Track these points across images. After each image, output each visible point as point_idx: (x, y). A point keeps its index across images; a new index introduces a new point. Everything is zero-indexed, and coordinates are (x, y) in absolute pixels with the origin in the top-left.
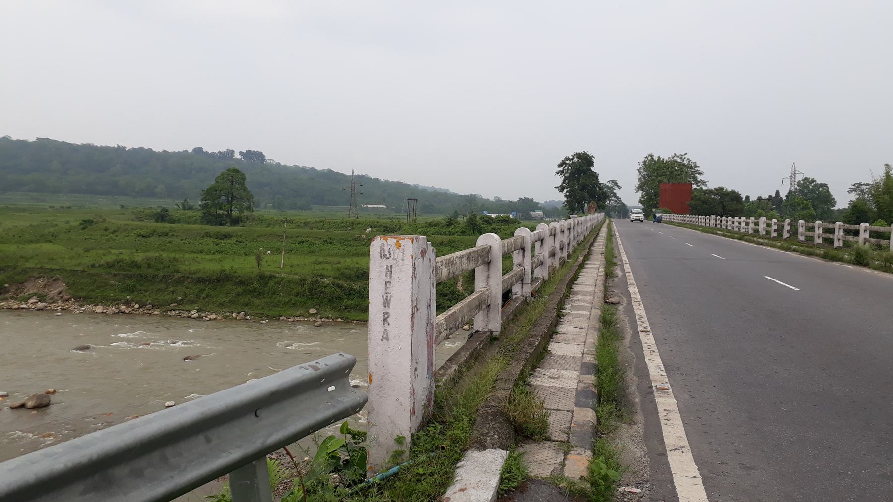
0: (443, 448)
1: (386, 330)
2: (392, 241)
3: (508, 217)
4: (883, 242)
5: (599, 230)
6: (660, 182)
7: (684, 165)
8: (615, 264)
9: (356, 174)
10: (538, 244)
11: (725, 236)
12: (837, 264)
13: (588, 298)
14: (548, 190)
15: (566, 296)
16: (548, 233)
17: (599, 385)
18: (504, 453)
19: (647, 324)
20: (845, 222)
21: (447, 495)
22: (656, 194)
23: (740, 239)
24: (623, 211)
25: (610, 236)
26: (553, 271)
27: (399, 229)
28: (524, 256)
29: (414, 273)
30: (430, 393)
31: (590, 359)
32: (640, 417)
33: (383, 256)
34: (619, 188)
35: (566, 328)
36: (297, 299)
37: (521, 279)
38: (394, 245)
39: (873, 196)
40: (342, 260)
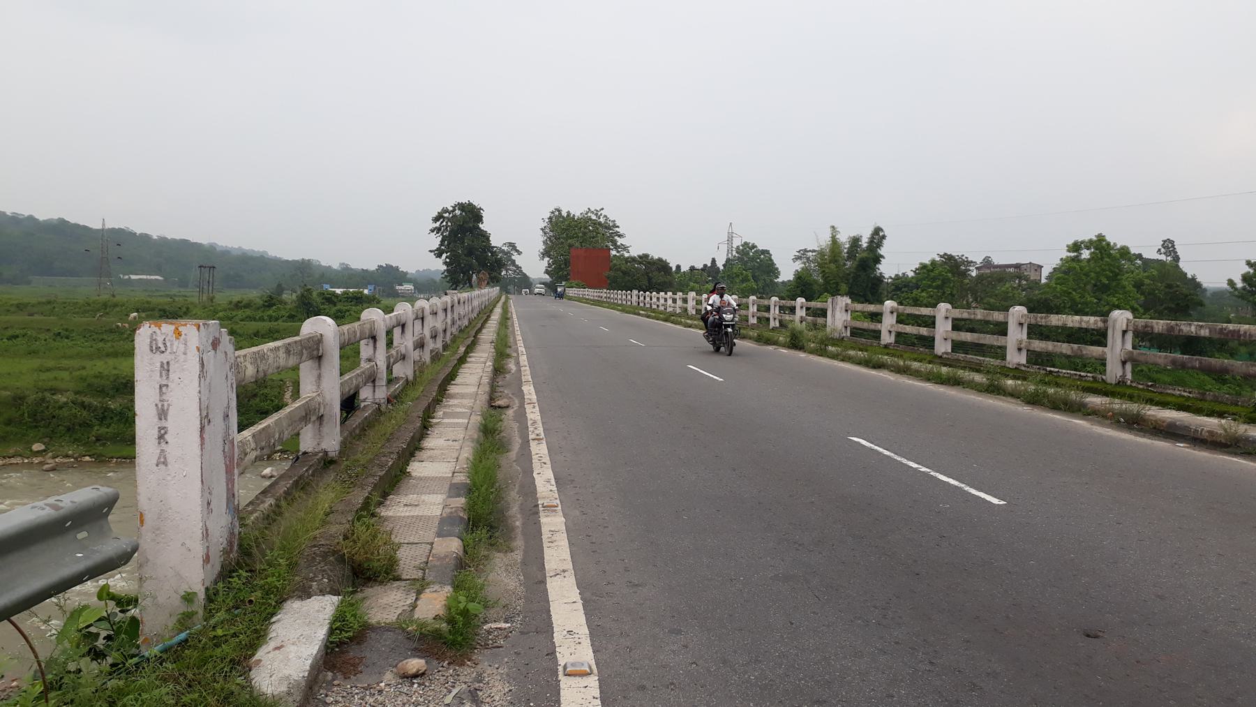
0: (251, 602)
1: (162, 451)
2: (167, 328)
3: (346, 295)
4: (820, 320)
5: (491, 311)
6: (570, 246)
7: (600, 224)
8: (509, 356)
9: (109, 226)
10: (397, 331)
11: (648, 317)
12: (771, 348)
13: (468, 402)
14: (421, 255)
15: (437, 401)
16: (411, 316)
17: (471, 508)
18: (336, 599)
19: (541, 430)
20: (781, 298)
21: (257, 657)
22: (567, 263)
23: (666, 320)
24: (524, 282)
25: (505, 318)
26: (420, 368)
27: (185, 314)
28: (375, 348)
29: (202, 371)
30: (232, 534)
31: (461, 478)
32: (519, 543)
33: (155, 349)
34: (519, 253)
35: (433, 442)
36: (8, 429)
37: (372, 379)
38: (171, 333)
39: (820, 265)
40: (88, 364)
